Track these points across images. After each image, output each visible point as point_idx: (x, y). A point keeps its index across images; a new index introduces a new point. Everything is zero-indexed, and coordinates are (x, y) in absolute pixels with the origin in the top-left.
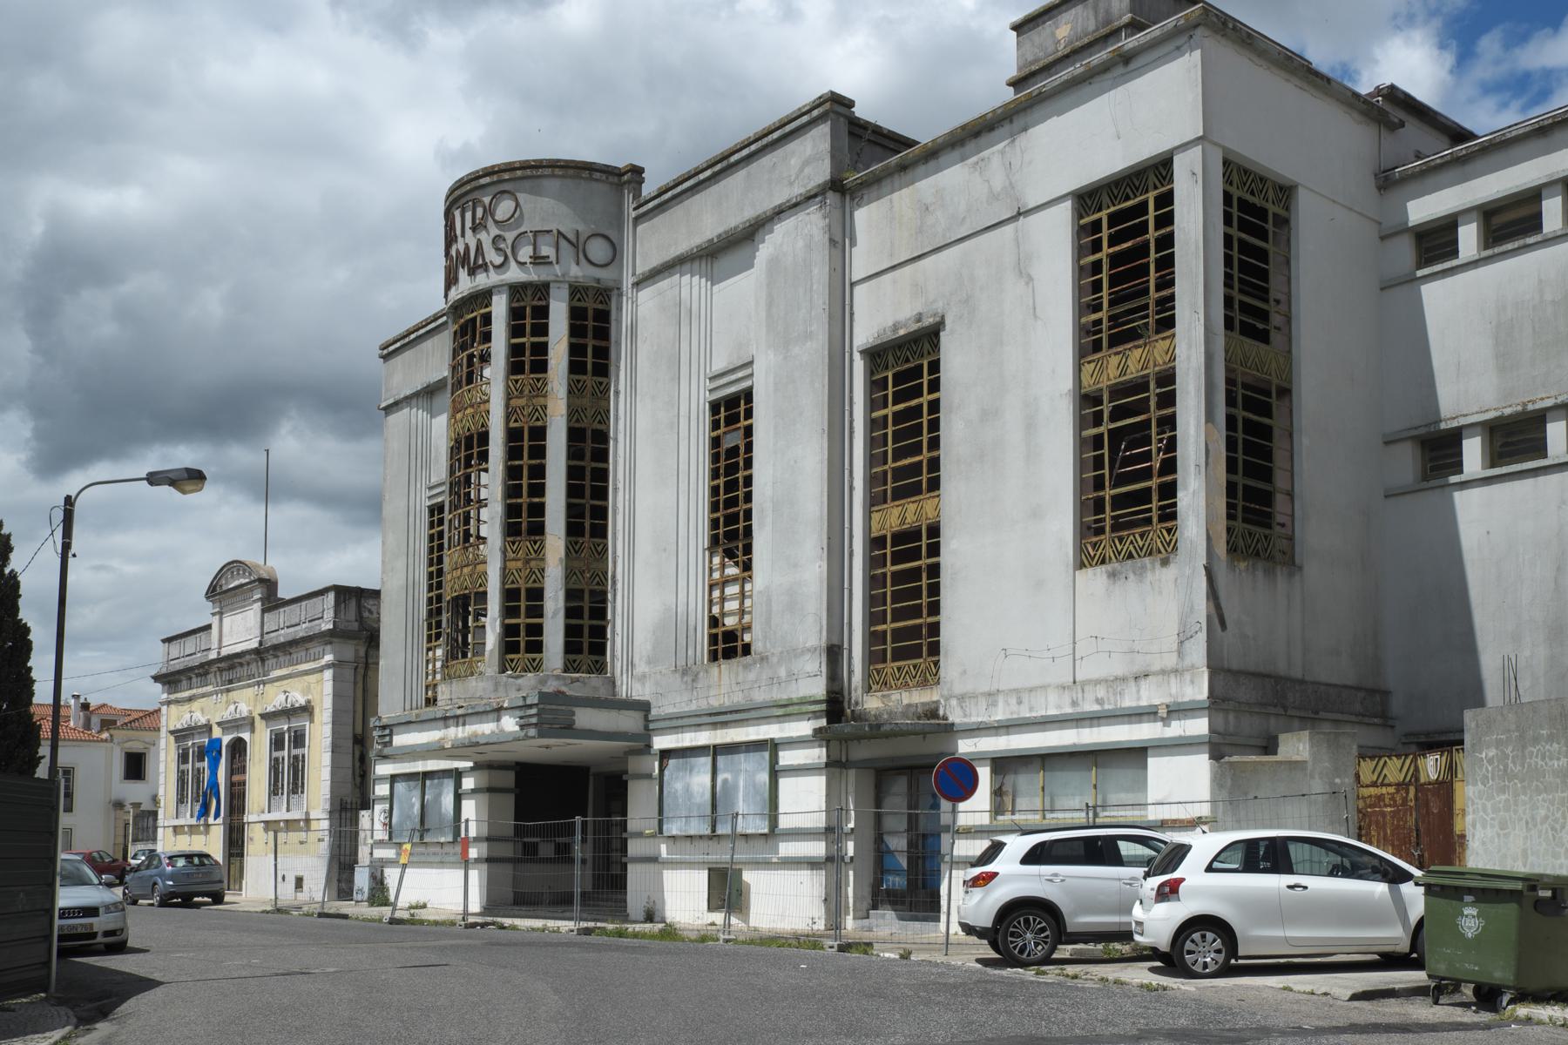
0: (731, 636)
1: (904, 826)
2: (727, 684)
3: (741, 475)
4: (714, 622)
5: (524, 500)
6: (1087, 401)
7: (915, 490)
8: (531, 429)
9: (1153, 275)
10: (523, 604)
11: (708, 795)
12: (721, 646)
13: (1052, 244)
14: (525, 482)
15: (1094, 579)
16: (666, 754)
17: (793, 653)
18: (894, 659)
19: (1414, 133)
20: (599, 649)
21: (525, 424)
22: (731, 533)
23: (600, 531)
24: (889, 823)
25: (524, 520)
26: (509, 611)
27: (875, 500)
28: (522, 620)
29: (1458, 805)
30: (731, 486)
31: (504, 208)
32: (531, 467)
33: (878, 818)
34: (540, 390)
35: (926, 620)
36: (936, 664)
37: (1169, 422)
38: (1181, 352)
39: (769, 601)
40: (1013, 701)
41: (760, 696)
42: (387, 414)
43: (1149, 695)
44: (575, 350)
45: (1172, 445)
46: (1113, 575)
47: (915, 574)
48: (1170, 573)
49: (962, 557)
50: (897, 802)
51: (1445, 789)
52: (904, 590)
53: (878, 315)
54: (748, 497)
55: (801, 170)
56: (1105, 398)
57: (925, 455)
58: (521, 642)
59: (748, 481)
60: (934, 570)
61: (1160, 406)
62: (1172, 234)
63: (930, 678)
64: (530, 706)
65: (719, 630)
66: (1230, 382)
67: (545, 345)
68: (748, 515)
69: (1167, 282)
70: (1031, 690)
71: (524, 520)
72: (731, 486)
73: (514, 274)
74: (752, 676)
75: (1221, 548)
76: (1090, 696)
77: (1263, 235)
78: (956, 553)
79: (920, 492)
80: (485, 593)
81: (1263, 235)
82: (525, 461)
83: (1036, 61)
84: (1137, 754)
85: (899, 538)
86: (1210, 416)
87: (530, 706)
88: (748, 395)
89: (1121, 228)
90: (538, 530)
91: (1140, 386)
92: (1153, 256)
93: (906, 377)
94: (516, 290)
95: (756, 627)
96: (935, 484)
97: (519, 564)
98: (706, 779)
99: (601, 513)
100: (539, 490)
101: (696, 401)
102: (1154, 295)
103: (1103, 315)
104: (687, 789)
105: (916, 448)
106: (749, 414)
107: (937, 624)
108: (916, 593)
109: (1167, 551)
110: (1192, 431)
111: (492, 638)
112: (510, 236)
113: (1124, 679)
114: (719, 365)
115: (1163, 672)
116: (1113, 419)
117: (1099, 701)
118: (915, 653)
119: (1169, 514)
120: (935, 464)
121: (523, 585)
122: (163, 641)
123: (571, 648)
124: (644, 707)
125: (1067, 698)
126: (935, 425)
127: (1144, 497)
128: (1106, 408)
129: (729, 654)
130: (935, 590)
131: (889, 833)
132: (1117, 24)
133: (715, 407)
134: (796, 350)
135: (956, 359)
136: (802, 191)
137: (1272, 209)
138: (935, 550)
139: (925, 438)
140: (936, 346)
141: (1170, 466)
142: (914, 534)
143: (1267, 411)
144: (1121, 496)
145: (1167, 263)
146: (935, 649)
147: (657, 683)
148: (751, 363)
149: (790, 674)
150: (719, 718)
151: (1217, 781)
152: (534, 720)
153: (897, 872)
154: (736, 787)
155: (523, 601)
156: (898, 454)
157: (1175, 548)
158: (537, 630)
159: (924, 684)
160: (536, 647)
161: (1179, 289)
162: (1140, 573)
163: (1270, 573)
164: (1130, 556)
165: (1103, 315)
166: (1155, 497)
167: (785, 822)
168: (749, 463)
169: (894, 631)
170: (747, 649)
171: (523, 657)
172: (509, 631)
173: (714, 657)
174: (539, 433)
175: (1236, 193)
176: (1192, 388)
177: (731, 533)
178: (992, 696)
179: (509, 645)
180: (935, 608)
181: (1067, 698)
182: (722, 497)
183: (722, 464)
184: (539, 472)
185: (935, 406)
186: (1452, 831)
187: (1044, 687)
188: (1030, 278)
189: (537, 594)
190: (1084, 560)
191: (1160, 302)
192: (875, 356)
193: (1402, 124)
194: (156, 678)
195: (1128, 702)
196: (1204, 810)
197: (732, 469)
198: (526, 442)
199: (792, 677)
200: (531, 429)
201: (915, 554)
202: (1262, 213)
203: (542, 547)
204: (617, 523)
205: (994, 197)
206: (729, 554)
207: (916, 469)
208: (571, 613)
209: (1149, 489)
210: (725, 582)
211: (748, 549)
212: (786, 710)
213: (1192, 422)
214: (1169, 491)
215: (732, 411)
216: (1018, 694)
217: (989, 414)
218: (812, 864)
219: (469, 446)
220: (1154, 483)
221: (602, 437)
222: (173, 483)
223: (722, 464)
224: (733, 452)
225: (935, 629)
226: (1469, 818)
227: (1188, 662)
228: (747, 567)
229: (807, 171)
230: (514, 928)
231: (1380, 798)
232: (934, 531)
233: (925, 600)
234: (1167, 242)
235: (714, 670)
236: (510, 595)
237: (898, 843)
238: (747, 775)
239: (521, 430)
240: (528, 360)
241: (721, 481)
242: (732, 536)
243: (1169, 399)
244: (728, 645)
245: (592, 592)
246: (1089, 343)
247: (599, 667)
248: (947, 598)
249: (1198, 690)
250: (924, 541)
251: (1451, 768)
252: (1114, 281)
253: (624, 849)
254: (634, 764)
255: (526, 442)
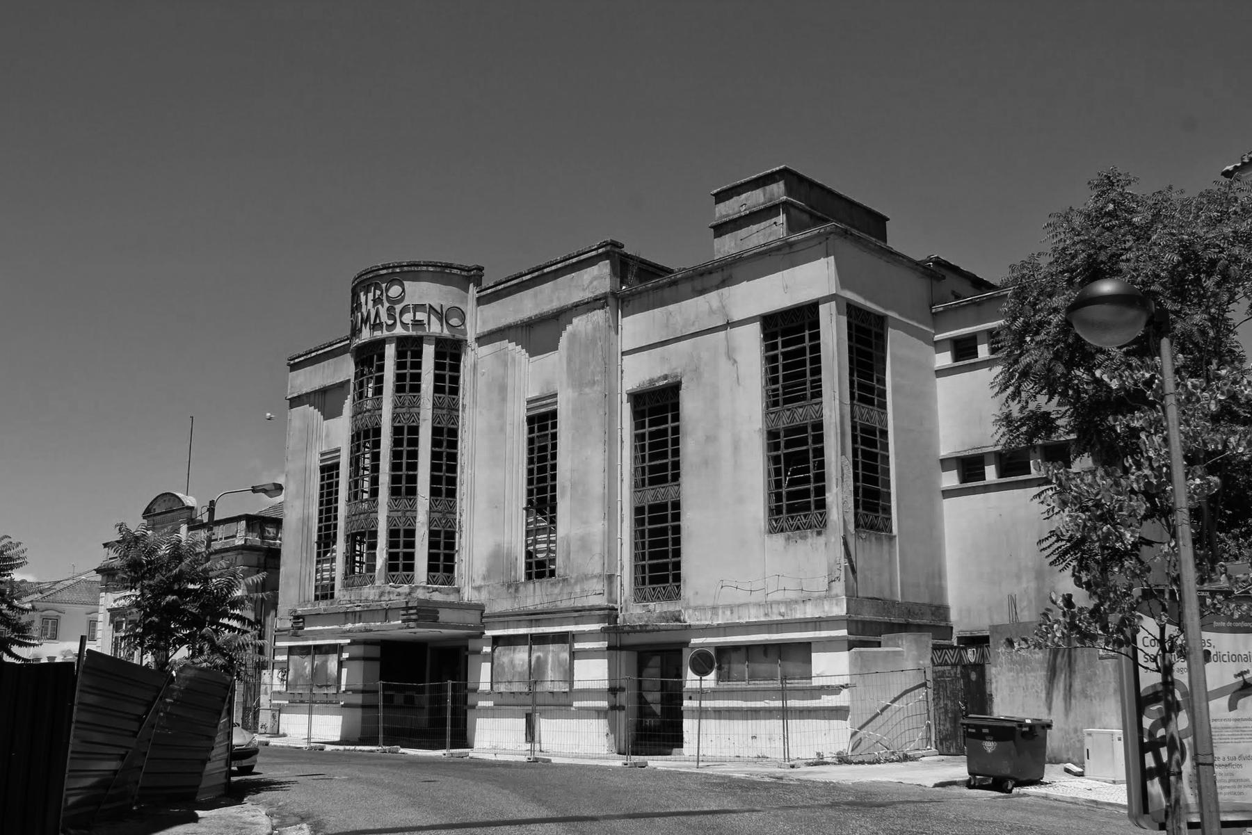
0: (541, 564)
1: (659, 687)
2: (535, 596)
3: (549, 463)
4: (529, 554)
5: (404, 472)
6: (772, 435)
7: (663, 480)
8: (409, 428)
9: (808, 367)
10: (402, 539)
11: (526, 666)
12: (534, 570)
13: (750, 341)
14: (404, 461)
15: (779, 539)
16: (496, 641)
17: (585, 578)
18: (651, 583)
19: (951, 282)
20: (450, 569)
21: (405, 424)
22: (542, 500)
23: (452, 493)
24: (646, 685)
25: (403, 485)
26: (392, 544)
27: (639, 485)
28: (401, 550)
29: (987, 678)
30: (542, 470)
31: (395, 291)
32: (402, 445)
33: (640, 683)
34: (416, 404)
35: (671, 559)
36: (678, 587)
37: (820, 452)
38: (826, 412)
39: (569, 545)
40: (728, 613)
41: (565, 604)
42: (291, 407)
43: (810, 612)
44: (438, 378)
45: (821, 465)
46: (788, 538)
47: (664, 531)
48: (822, 539)
49: (696, 524)
50: (653, 676)
51: (980, 668)
52: (659, 549)
53: (638, 373)
54: (554, 477)
55: (591, 282)
56: (782, 434)
57: (670, 460)
58: (400, 564)
59: (554, 467)
60: (677, 530)
61: (814, 442)
62: (819, 345)
63: (676, 595)
64: (411, 608)
65: (533, 560)
66: (854, 428)
67: (420, 375)
68: (554, 488)
69: (817, 371)
70: (739, 606)
71: (403, 485)
72: (542, 470)
73: (399, 331)
74: (557, 591)
75: (851, 527)
76: (775, 610)
77: (869, 345)
78: (691, 520)
79: (666, 481)
80: (376, 532)
81: (869, 345)
82: (405, 448)
83: (728, 215)
84: (805, 649)
85: (653, 508)
86: (843, 453)
87: (411, 608)
88: (554, 414)
89: (789, 331)
90: (412, 491)
91: (803, 429)
92: (808, 356)
93: (658, 408)
94: (401, 342)
95: (559, 561)
96: (676, 477)
97: (400, 514)
98: (526, 656)
99: (452, 481)
100: (413, 467)
101: (518, 415)
102: (809, 378)
103: (779, 386)
104: (512, 662)
105: (665, 455)
106: (554, 426)
107: (679, 562)
108: (665, 543)
109: (821, 526)
110: (833, 459)
111: (380, 561)
112: (398, 308)
113: (796, 602)
114: (534, 394)
115: (819, 598)
116: (786, 447)
117: (780, 614)
118: (664, 580)
119: (821, 505)
120: (676, 465)
121: (402, 527)
122: (105, 545)
123: (432, 568)
124: (480, 608)
125: (762, 611)
126: (676, 442)
127: (806, 493)
128: (782, 440)
129: (540, 575)
130: (677, 541)
131: (785, 728)
132: (777, 202)
133: (531, 420)
134: (587, 390)
135: (689, 404)
136: (592, 295)
137: (874, 329)
138: (677, 517)
139: (670, 449)
140: (677, 395)
141: (821, 477)
142: (663, 507)
143: (873, 444)
144: (794, 497)
145: (817, 360)
146: (677, 578)
147: (489, 593)
148: (555, 395)
149: (583, 591)
150: (534, 617)
151: (853, 663)
152: (414, 617)
153: (654, 714)
154: (546, 661)
155: (402, 538)
156: (652, 458)
157: (825, 525)
158: (411, 556)
159: (669, 598)
160: (410, 568)
161: (824, 375)
162: (804, 538)
163: (879, 539)
164: (798, 528)
165: (779, 386)
166: (812, 495)
167: (577, 686)
168: (554, 457)
169: (650, 565)
170: (552, 573)
171: (401, 573)
172: (392, 557)
173: (529, 576)
174: (414, 430)
175: (854, 322)
176: (832, 433)
177: (542, 500)
178: (714, 608)
179: (392, 567)
180: (677, 553)
181: (762, 611)
182: (535, 476)
183: (535, 455)
184: (414, 455)
185: (676, 430)
186: (985, 692)
187: (746, 605)
188: (735, 362)
189: (411, 533)
190: (772, 530)
191: (812, 382)
192: (638, 399)
193: (944, 277)
194: (98, 571)
195: (799, 615)
196: (845, 680)
197: (543, 459)
198: (406, 435)
199: (584, 593)
200: (409, 428)
201: (664, 519)
202: (868, 332)
203: (415, 503)
204: (462, 490)
205: (712, 312)
206: (541, 512)
207: (664, 467)
208: (432, 545)
209: (808, 490)
210: (538, 531)
211: (554, 510)
212: (580, 614)
213: (833, 454)
214: (821, 491)
215: (542, 424)
216: (732, 608)
217: (711, 439)
218: (599, 713)
219: (367, 436)
220: (812, 486)
221: (454, 433)
222: (265, 491)
223: (535, 455)
224: (544, 449)
225: (677, 566)
226: (994, 686)
227: (834, 592)
228: (553, 521)
229: (595, 283)
230: (1025, 795)
231: (944, 672)
232: (677, 505)
233: (670, 548)
234: (816, 349)
235: (531, 586)
236: (393, 533)
237: (653, 697)
238: (554, 654)
239: (402, 428)
240: (408, 384)
241: (535, 466)
242: (542, 501)
243: (819, 439)
244: (539, 569)
245: (446, 532)
246: (772, 402)
247: (450, 581)
248: (685, 547)
249: (840, 609)
250: (670, 512)
251: (983, 656)
252: (785, 367)
253: (466, 702)
254: (472, 644)
255: (406, 435)
